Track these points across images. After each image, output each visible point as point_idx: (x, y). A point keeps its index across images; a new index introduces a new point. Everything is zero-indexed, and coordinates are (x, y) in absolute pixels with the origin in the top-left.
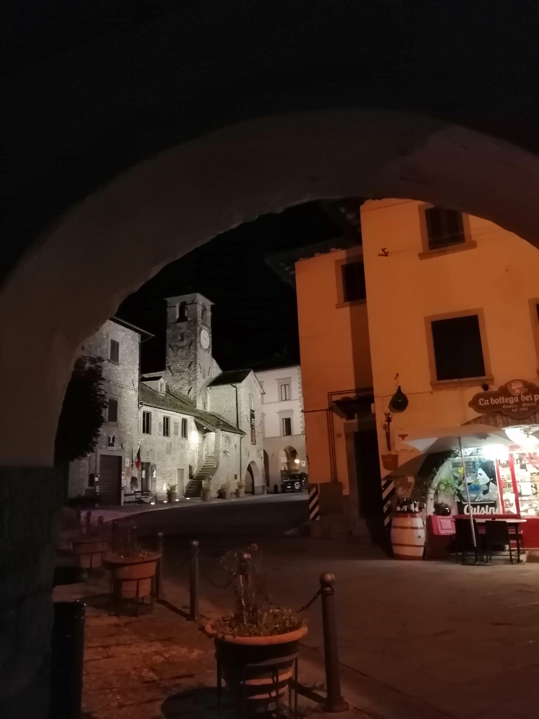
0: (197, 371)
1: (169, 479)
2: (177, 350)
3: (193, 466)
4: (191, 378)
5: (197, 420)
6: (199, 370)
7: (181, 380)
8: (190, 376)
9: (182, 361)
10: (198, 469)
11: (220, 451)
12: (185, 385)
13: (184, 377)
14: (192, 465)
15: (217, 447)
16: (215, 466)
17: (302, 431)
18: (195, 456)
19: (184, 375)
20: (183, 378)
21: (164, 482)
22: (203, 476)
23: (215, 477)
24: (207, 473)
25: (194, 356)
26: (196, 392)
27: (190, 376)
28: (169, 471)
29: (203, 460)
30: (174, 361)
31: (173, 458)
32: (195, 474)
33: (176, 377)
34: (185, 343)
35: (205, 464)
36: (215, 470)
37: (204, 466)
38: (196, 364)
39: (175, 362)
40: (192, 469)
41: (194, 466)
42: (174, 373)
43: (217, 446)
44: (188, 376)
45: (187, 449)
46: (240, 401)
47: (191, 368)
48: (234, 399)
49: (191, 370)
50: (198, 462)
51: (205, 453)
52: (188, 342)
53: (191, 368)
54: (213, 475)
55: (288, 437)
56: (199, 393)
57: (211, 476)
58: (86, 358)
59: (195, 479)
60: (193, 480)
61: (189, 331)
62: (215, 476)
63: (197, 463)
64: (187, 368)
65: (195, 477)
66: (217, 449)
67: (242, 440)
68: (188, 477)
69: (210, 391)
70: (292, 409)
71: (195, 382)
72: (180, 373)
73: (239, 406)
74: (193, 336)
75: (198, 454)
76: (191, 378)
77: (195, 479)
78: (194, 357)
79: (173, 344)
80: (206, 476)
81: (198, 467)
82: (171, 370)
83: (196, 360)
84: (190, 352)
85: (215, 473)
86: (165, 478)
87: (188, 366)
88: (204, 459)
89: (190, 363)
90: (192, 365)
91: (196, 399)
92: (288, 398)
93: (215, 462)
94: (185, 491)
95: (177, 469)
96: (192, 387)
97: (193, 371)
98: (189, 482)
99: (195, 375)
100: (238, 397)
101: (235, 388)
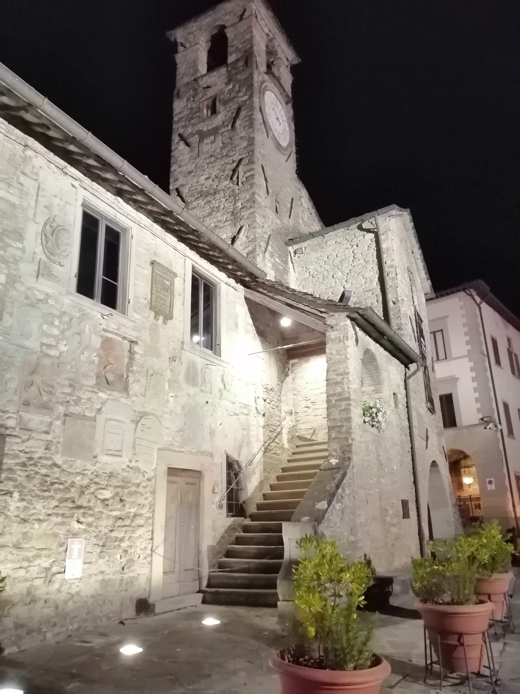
0: (256, 181)
1: (115, 513)
2: (201, 141)
3: (243, 465)
4: (239, 204)
5: (256, 297)
6: (259, 180)
7: (210, 214)
8: (234, 197)
9: (211, 166)
10: (267, 479)
11: (352, 397)
12: (222, 227)
13: (219, 206)
14: (243, 460)
15: (336, 383)
16: (334, 461)
17: (481, 417)
18: (253, 428)
19: (218, 202)
20: (215, 209)
21: (75, 535)
22: (285, 506)
23: (338, 506)
24: (303, 493)
25: (245, 144)
26: (254, 240)
27: (234, 197)
28: (111, 475)
29: (282, 448)
30: (190, 173)
31: (143, 415)
32: (250, 498)
33: (195, 211)
34: (219, 119)
35: (294, 454)
36: (339, 476)
37: (284, 470)
38: (251, 162)
39: (193, 174)
40: (241, 475)
41: (250, 463)
42: (191, 202)
43: (339, 379)
44: (230, 200)
45: (215, 391)
46: (391, 266)
47: (238, 178)
48: (369, 267)
49: (238, 184)
50: (265, 452)
51: (287, 423)
52: (229, 114)
53: (238, 178)
54: (331, 498)
55: (451, 432)
56: (263, 245)
57: (322, 505)
58: (458, 681)
59: (253, 517)
60: (247, 522)
61: (231, 86)
62: (338, 501)
63: (261, 453)
64: (226, 179)
65: (252, 509)
66: (339, 390)
67: (410, 381)
68: (221, 507)
69: (296, 258)
70: (454, 376)
71: (252, 210)
72: (208, 198)
73: (389, 283)
74: (241, 94)
75: (262, 421)
76: (239, 204)
77: (253, 517)
78: (245, 147)
79: (190, 130)
80: (299, 502)
81: (265, 470)
82: (184, 196)
83: (251, 153)
84: (235, 137)
85: (340, 490)
86: (80, 507)
87: (231, 173)
88: (286, 445)
89: (235, 164)
90: (241, 169)
91: (254, 258)
92: (442, 355)
93: (335, 446)
94: (206, 571)
95: (164, 469)
96: (241, 228)
97: (242, 183)
98: (231, 528)
99: (251, 191)
100: (385, 257)
101: (372, 236)
